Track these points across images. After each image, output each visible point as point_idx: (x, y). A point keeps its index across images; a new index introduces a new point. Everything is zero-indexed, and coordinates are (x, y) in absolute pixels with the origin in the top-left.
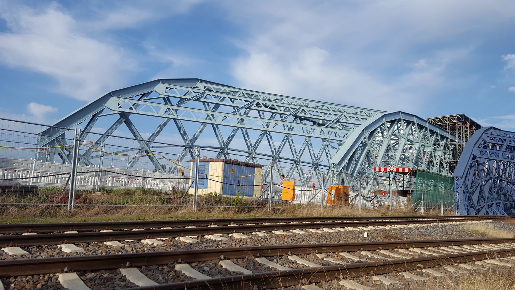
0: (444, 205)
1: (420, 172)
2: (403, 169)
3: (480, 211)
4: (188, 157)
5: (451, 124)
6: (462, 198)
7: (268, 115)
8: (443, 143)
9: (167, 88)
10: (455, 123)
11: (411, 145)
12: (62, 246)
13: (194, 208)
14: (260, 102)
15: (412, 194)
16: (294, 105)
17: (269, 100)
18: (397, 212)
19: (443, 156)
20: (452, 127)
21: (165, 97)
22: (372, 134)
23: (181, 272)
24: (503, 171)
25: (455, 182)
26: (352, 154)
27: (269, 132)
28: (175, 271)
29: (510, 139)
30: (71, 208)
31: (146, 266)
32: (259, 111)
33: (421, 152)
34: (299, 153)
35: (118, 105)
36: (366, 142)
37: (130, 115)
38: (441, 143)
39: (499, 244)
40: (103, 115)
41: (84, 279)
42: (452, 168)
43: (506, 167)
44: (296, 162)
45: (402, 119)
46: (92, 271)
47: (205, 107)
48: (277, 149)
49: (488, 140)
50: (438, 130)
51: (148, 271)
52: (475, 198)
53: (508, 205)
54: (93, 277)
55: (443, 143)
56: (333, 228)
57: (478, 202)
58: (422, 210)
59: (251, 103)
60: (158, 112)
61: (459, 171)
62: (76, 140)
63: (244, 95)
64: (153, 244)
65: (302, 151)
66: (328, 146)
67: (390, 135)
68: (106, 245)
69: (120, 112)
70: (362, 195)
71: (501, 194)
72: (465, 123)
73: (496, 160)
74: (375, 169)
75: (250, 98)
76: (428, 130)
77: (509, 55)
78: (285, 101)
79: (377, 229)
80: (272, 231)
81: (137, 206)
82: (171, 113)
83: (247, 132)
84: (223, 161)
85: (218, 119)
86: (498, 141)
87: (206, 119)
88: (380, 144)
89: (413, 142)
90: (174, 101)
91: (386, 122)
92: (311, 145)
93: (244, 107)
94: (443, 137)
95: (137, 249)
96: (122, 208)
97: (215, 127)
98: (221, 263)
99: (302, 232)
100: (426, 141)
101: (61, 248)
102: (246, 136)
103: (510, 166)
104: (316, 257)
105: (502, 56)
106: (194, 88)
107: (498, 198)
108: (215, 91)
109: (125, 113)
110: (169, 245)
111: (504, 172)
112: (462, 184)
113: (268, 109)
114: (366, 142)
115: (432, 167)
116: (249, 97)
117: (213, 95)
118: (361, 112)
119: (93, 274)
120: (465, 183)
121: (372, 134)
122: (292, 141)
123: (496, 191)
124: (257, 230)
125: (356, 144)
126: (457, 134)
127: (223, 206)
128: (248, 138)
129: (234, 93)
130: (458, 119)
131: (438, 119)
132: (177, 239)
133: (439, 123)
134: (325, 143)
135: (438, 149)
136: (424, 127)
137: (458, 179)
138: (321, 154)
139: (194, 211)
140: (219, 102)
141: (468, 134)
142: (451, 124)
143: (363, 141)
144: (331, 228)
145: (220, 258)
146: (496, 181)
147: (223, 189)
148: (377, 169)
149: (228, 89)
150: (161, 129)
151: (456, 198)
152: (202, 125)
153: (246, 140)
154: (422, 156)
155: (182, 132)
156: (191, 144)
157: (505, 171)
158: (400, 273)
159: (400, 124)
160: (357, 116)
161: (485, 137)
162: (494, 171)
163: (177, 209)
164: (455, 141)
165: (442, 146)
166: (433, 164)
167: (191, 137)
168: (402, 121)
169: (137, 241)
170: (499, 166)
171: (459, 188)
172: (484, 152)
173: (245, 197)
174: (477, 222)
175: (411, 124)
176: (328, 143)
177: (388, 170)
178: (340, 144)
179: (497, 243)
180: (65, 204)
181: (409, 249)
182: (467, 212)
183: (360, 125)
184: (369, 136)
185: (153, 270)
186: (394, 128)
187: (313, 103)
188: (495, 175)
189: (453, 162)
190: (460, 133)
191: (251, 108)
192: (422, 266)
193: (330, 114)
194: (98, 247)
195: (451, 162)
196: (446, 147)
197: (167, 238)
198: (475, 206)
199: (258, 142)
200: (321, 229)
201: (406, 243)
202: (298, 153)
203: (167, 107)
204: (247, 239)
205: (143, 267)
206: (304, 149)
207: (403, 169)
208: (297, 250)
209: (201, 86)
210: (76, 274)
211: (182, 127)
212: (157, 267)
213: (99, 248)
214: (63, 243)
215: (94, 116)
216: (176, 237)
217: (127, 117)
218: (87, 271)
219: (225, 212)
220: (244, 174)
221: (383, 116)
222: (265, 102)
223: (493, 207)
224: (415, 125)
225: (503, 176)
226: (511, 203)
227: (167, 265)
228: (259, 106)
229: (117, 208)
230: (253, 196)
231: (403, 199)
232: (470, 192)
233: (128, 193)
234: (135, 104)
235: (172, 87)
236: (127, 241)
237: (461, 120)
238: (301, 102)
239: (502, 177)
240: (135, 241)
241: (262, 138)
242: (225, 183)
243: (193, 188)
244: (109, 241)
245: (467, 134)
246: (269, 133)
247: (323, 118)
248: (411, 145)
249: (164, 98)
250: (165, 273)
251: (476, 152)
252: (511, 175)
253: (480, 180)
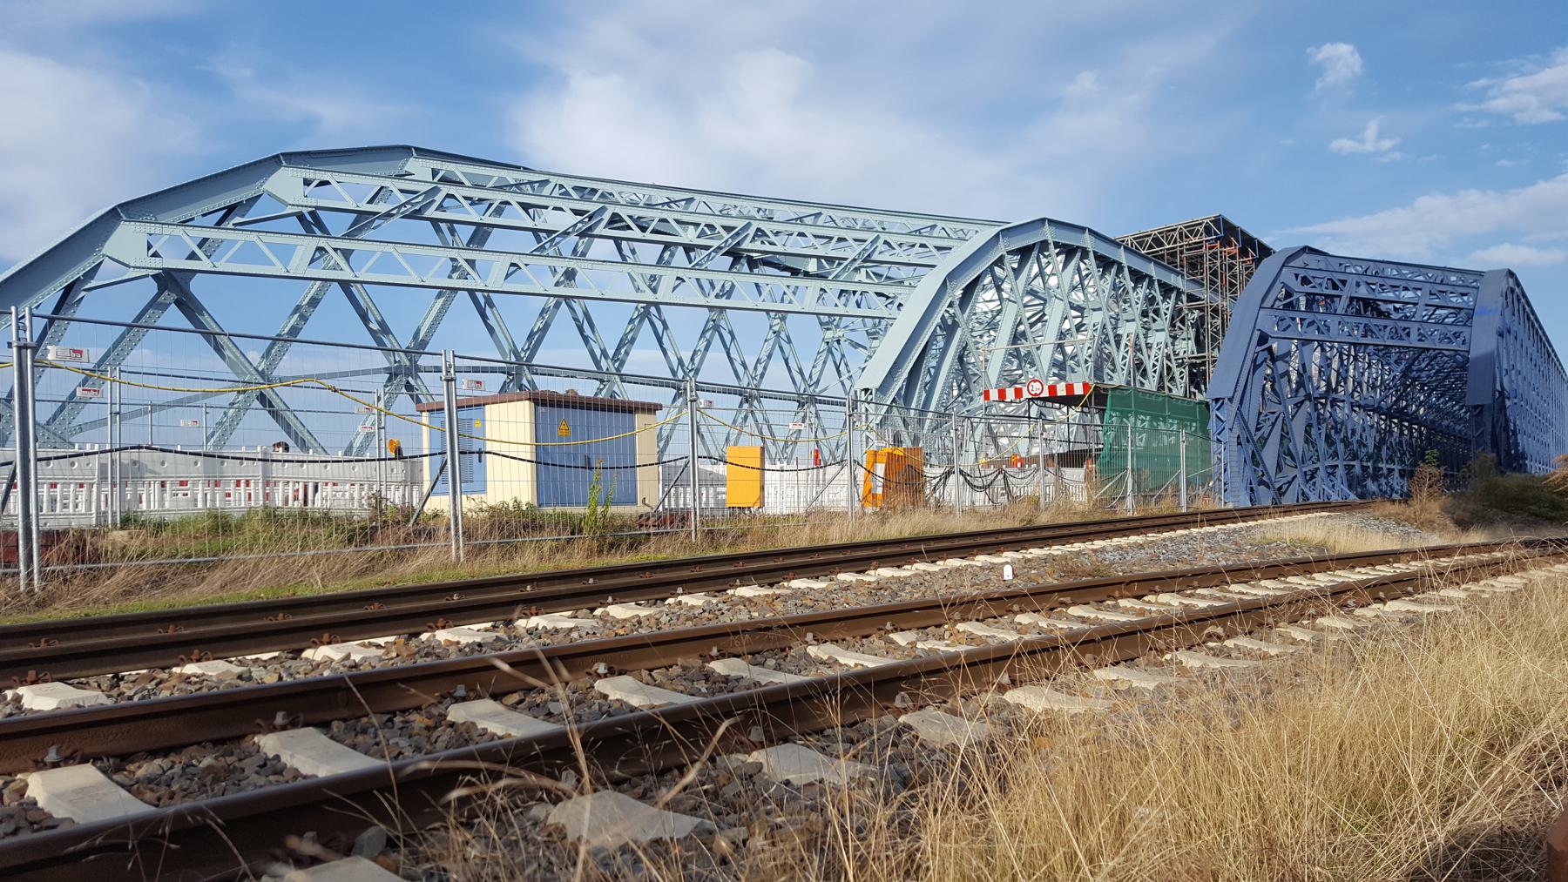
0: (1189, 483)
1: (1117, 393)
2: (1070, 387)
3: (1284, 493)
4: (404, 402)
5: (1187, 250)
6: (1235, 459)
7: (650, 253)
8: (1166, 307)
9: (307, 182)
10: (1199, 246)
11: (1080, 319)
12: (21, 690)
13: (456, 549)
14: (624, 212)
15: (1097, 456)
16: (728, 216)
17: (649, 206)
18: (1064, 514)
19: (1169, 344)
20: (1191, 258)
21: (305, 210)
22: (969, 290)
23: (474, 724)
24: (1339, 374)
25: (1213, 413)
26: (913, 362)
27: (656, 305)
28: (452, 725)
29: (1356, 278)
30: (32, 580)
31: (344, 720)
32: (618, 241)
33: (1109, 336)
34: (755, 368)
35: (149, 249)
36: (953, 316)
37: (191, 279)
38: (1163, 307)
39: (1377, 567)
40: (100, 283)
41: (127, 782)
42: (1197, 378)
43: (1345, 362)
44: (748, 397)
45: (1051, 241)
46: (153, 754)
47: (443, 239)
48: (686, 361)
49: (1296, 285)
50: (1151, 269)
51: (356, 735)
52: (1270, 455)
53: (1357, 470)
54: (160, 772)
55: (1166, 307)
56: (906, 567)
57: (1279, 468)
58: (1129, 501)
59: (590, 218)
60: (285, 264)
61: (1221, 382)
62: (20, 348)
63: (567, 193)
64: (348, 657)
65: (764, 362)
66: (838, 341)
67: (1021, 292)
68: (181, 675)
69: (157, 272)
70: (961, 472)
71: (1338, 441)
72: (1226, 242)
73: (1321, 344)
74: (987, 395)
75: (590, 200)
76: (1126, 270)
77: (1327, 47)
78: (699, 204)
79: (1029, 556)
80: (725, 590)
81: (262, 558)
82: (332, 262)
83: (587, 315)
84: (529, 399)
85: (491, 272)
86: (1325, 285)
87: (450, 277)
88: (993, 325)
89: (1084, 309)
90: (338, 224)
91: (1009, 253)
92: (789, 341)
93: (573, 231)
94: (1167, 289)
95: (297, 676)
96: (211, 567)
97: (482, 303)
98: (601, 686)
99: (818, 585)
100: (1121, 303)
101: (18, 699)
102: (586, 327)
103: (1355, 359)
104: (892, 642)
105: (1309, 50)
106: (400, 176)
107: (1330, 452)
108: (467, 184)
109: (173, 273)
110: (405, 654)
111: (1342, 378)
112: (1233, 417)
113: (648, 235)
114: (953, 316)
115: (1142, 380)
116: (582, 199)
117: (466, 198)
118: (933, 227)
119: (158, 762)
120: (1242, 416)
121: (969, 290)
122: (731, 333)
123: (1323, 432)
124: (680, 590)
125: (921, 334)
126: (1207, 276)
127: (548, 538)
128: (593, 332)
129: (533, 189)
130: (1208, 230)
131: (1150, 235)
132: (424, 637)
133: (1155, 247)
134: (829, 334)
135: (1154, 326)
136: (1114, 262)
137: (1223, 403)
138: (819, 368)
139: (458, 557)
140: (487, 219)
141: (1235, 276)
142: (1187, 250)
143: (947, 315)
144: (899, 567)
145: (596, 671)
146: (1321, 404)
147: (540, 486)
148: (994, 395)
149: (511, 177)
150: (304, 318)
151: (1219, 459)
152: (439, 296)
153: (586, 339)
154: (1112, 348)
155: (375, 326)
156: (408, 363)
157: (1344, 375)
158: (1168, 656)
159: (1045, 257)
160: (924, 241)
161: (1288, 276)
162: (1315, 379)
163: (399, 556)
164: (1200, 299)
165: (1166, 314)
166: (1145, 370)
167: (406, 341)
168: (1052, 247)
169: (290, 655)
170: (1328, 358)
171: (1226, 430)
172: (1288, 321)
173: (613, 510)
174: (1303, 517)
175: (1078, 255)
176: (839, 333)
177: (1026, 395)
178: (874, 333)
179: (1372, 565)
180: (9, 570)
181: (1146, 598)
182: (1251, 500)
183: (934, 266)
184: (964, 294)
185: (372, 730)
186: (1031, 269)
187: (786, 207)
188: (1318, 388)
189: (1198, 361)
190: (1214, 274)
191: (596, 232)
192: (1220, 630)
193: (841, 240)
194: (154, 683)
195: (1194, 361)
196: (1177, 316)
197: (391, 639)
198: (1271, 480)
199: (626, 342)
200: (872, 572)
201: (1134, 581)
202: (751, 367)
203: (312, 243)
204: (657, 616)
205: (335, 724)
206: (769, 356)
207: (1070, 387)
208: (827, 625)
209: (420, 169)
210: (94, 768)
211: (373, 309)
212: (386, 717)
213: (161, 686)
214: (23, 683)
215: (68, 290)
216: (420, 634)
217: (182, 283)
218: (132, 754)
219: (558, 556)
220: (602, 433)
221: (998, 234)
222: (636, 212)
223: (1318, 479)
224: (1087, 258)
225: (1340, 389)
226: (1365, 464)
227: (418, 709)
228: (619, 225)
229: (193, 568)
230: (635, 502)
231: (1074, 474)
232: (1256, 438)
233: (221, 525)
234: (205, 240)
235: (326, 176)
236: (254, 657)
237: (1216, 234)
238: (749, 208)
239: (1337, 392)
240: (284, 655)
241: (636, 330)
242: (541, 461)
243: (446, 493)
244: (191, 661)
245: (1234, 276)
246: (659, 311)
247: (820, 252)
248: (1080, 319)
249: (300, 217)
250: (418, 734)
251: (1269, 324)
252: (1360, 384)
253: (1280, 404)
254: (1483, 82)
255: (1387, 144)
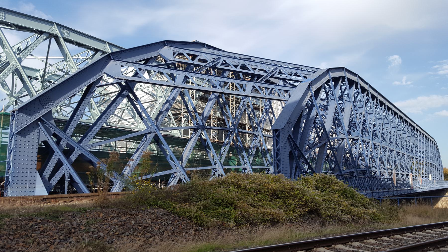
77: (391, 57)
235: (181, 51)
254: (437, 66)
255: (409, 83)
